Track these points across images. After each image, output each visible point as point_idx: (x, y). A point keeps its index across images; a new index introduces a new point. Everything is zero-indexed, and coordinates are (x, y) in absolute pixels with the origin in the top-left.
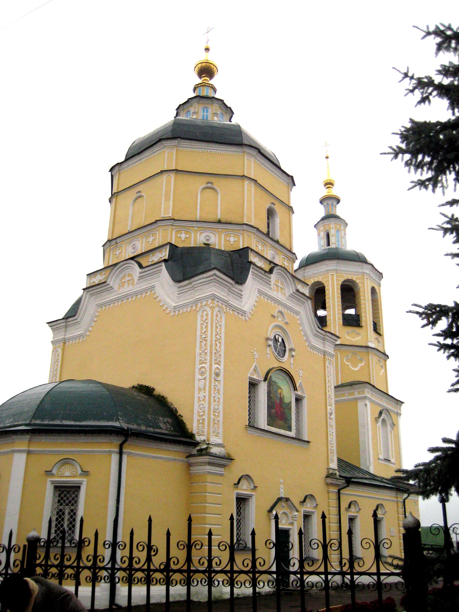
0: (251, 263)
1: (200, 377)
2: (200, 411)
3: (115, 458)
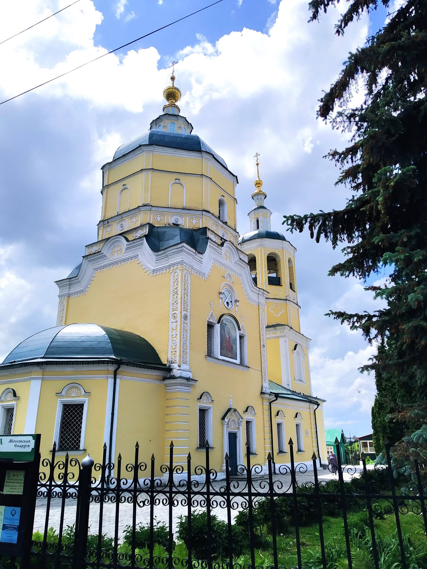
0: (208, 238)
1: (173, 321)
2: (173, 345)
3: (111, 381)
